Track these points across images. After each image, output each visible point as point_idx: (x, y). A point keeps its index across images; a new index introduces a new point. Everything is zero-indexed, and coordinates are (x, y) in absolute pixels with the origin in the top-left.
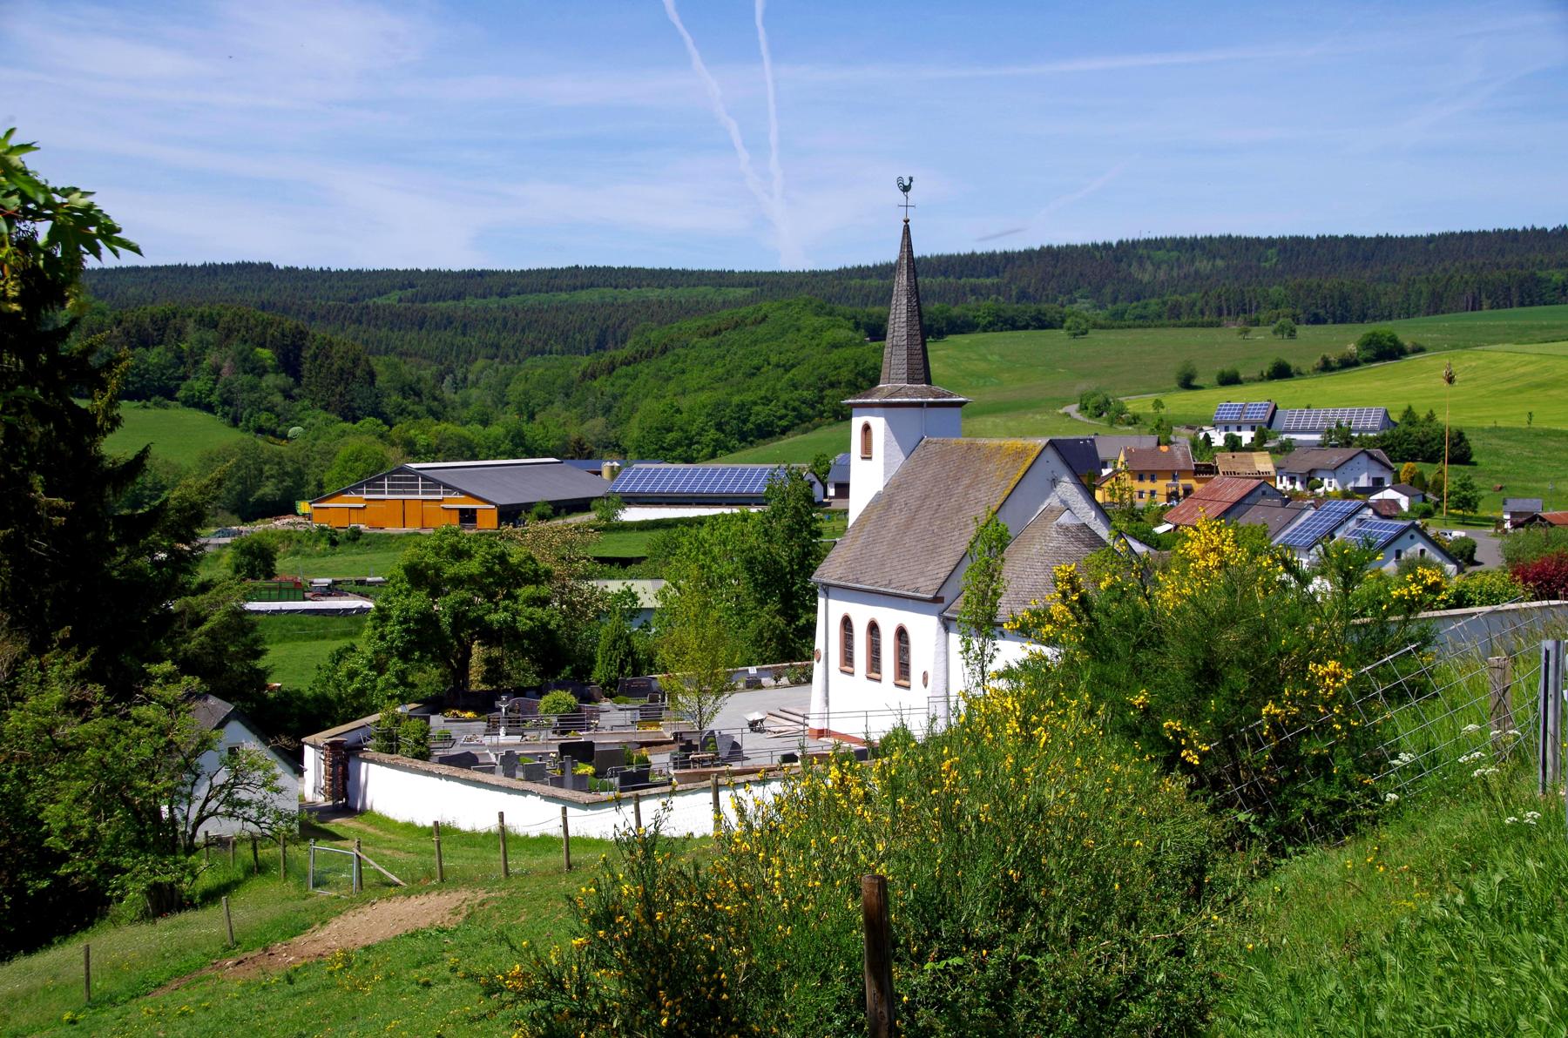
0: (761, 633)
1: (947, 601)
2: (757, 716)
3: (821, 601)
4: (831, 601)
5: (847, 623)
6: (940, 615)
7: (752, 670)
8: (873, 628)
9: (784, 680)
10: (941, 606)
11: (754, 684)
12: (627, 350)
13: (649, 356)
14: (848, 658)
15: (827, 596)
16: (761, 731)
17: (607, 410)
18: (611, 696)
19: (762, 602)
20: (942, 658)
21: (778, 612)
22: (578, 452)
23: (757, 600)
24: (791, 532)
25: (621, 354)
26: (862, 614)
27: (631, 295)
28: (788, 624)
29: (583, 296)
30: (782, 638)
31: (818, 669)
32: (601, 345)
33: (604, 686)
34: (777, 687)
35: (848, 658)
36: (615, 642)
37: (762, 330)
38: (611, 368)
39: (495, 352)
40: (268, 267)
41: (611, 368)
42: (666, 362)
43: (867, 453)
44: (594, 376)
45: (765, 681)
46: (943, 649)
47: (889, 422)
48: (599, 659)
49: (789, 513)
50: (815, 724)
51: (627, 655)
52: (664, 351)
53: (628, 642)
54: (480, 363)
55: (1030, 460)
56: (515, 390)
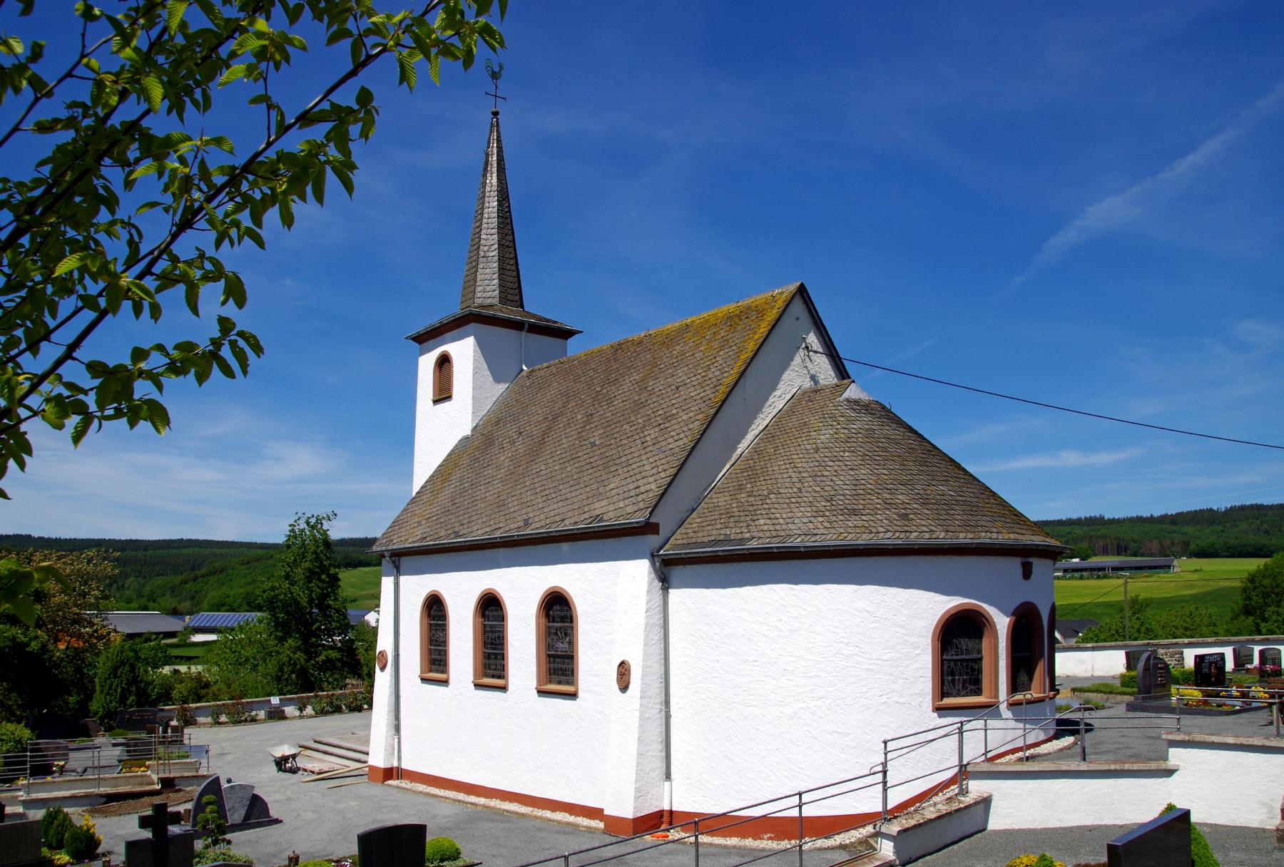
0: (281, 670)
1: (664, 531)
2: (287, 750)
3: (387, 583)
4: (403, 579)
5: (435, 608)
6: (653, 557)
7: (275, 700)
8: (490, 606)
9: (309, 710)
10: (653, 541)
11: (277, 715)
12: (203, 571)
13: (214, 573)
14: (436, 661)
15: (398, 571)
16: (294, 771)
17: (192, 598)
18: (109, 729)
19: (282, 640)
20: (657, 635)
21: (298, 648)
22: (175, 613)
23: (276, 638)
24: (311, 575)
25: (199, 573)
26: (461, 590)
27: (207, 551)
28: (307, 661)
29: (184, 551)
30: (302, 673)
31: (382, 680)
32: (193, 569)
33: (101, 719)
34: (301, 717)
35: (436, 661)
36: (115, 669)
37: (270, 562)
38: (195, 579)
39: (140, 574)
40: (29, 537)
41: (195, 579)
42: (223, 576)
43: (443, 393)
44: (186, 583)
45: (290, 710)
46: (658, 619)
47: (481, 344)
48: (98, 688)
49: (310, 557)
50: (378, 759)
51: (129, 684)
52: (222, 571)
53: (133, 668)
54: (131, 579)
55: (763, 329)
56: (148, 588)
